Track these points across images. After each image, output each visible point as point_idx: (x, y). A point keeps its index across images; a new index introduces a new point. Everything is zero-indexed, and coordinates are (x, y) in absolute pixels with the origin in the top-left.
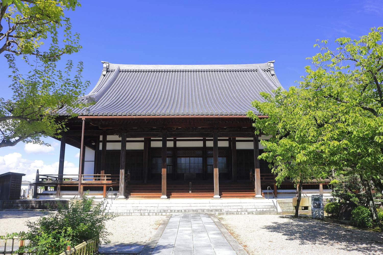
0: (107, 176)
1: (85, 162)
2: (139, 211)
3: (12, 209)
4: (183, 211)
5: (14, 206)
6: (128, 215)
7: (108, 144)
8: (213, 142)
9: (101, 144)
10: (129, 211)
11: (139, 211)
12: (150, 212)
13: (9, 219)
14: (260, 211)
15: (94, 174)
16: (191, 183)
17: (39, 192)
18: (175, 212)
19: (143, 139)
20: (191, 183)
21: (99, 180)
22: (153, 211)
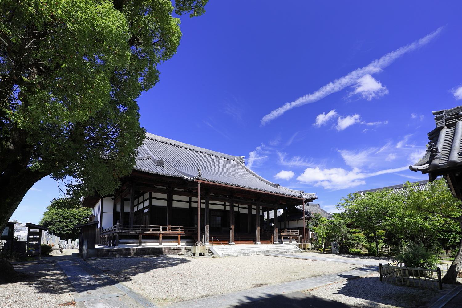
4: (262, 252)
18: (258, 253)
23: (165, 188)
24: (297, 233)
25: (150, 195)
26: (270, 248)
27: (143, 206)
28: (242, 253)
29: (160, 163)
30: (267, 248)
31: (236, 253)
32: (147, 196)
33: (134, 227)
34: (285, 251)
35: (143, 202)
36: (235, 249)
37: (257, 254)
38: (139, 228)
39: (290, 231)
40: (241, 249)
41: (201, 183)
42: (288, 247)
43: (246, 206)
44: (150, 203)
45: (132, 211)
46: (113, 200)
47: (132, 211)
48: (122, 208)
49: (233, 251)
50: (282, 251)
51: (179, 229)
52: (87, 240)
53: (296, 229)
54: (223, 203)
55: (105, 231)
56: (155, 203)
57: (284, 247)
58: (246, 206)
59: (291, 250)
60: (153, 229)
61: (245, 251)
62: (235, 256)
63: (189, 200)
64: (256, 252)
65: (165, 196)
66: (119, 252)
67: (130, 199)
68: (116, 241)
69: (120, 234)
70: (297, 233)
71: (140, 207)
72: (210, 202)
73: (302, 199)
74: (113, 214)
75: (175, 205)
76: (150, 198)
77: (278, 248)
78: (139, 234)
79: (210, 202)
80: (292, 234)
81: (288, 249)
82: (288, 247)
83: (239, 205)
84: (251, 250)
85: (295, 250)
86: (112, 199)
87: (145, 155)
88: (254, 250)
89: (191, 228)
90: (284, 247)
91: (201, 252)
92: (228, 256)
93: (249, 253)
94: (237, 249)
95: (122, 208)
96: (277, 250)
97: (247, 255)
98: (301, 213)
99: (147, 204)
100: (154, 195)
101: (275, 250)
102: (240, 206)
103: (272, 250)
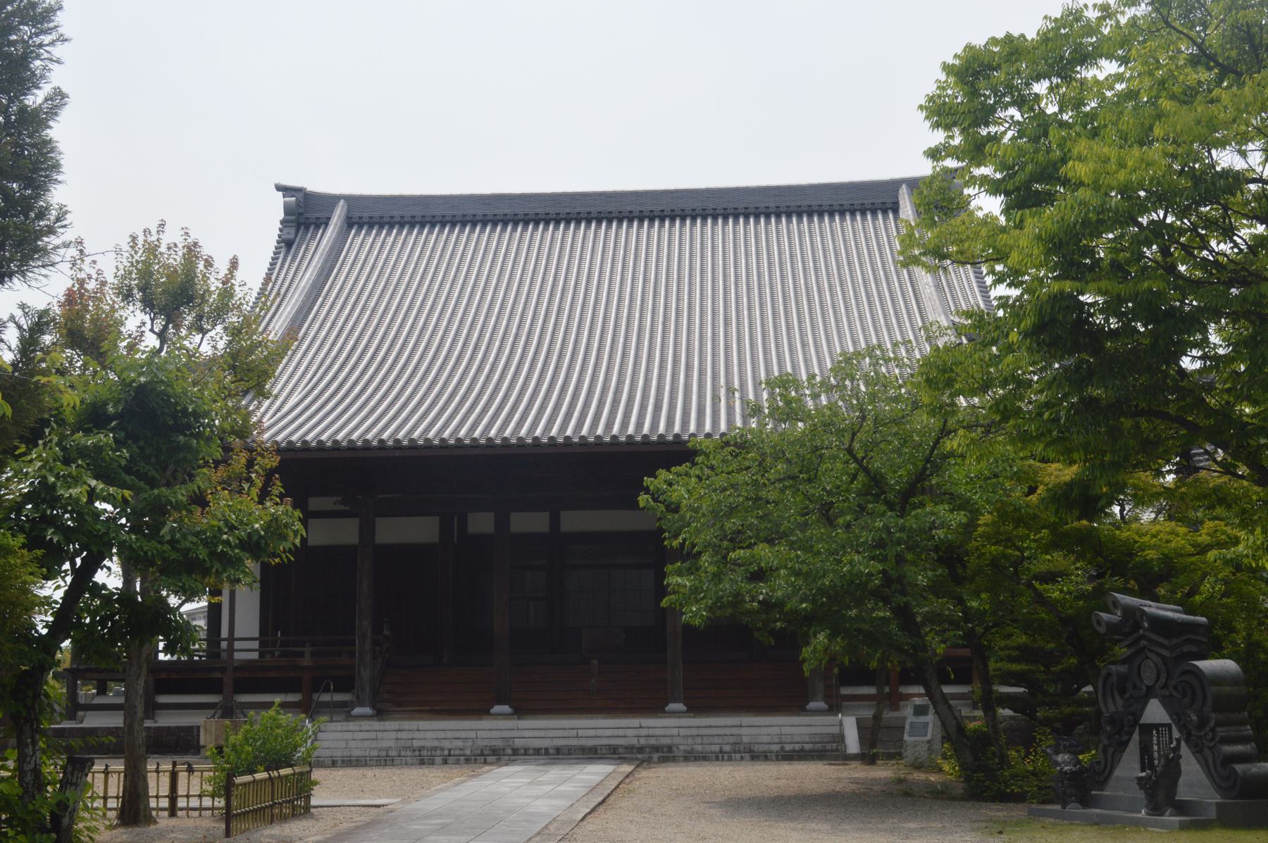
4: (551, 751)
16: (595, 662)
22: (458, 752)
51: (307, 650)
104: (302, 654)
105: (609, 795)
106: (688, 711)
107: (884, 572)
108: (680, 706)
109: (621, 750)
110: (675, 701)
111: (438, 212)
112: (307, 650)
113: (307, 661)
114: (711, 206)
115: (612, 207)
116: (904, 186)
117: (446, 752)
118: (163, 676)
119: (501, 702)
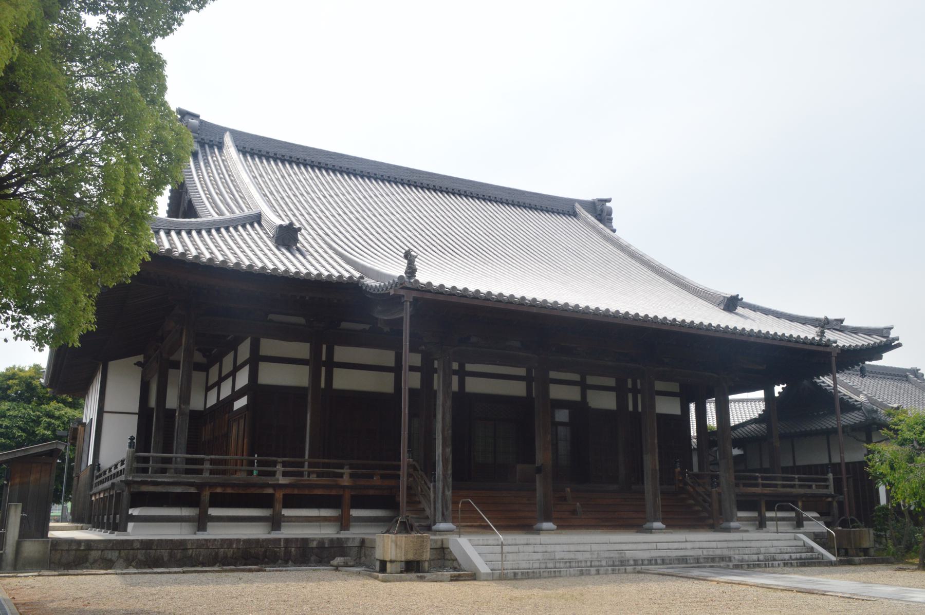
0: (800, 480)
1: (137, 411)
2: (568, 564)
3: (87, 568)
4: (659, 561)
5: (91, 560)
6: (553, 574)
7: (468, 380)
8: (336, 348)
9: (455, 379)
10: (543, 566)
11: (568, 564)
12: (591, 566)
13: (406, 583)
14: (801, 559)
15: (187, 453)
16: (568, 489)
17: (60, 514)
18: (643, 564)
19: (522, 372)
20: (568, 489)
21: (224, 472)
22: (597, 563)
23: (302, 320)
24: (827, 487)
25: (255, 347)
26: (697, 545)
27: (232, 387)
28: (573, 564)
29: (287, 237)
30: (683, 545)
31: (550, 565)
32: (244, 351)
33: (189, 461)
34: (761, 557)
35: (233, 374)
36: (549, 548)
37: (639, 568)
38: (274, 469)
39: (793, 479)
40: (572, 548)
41: (416, 300)
42: (775, 543)
43: (611, 382)
44: (253, 375)
45: (183, 407)
46: (140, 369)
47: (183, 407)
48: (184, 398)
49: (539, 556)
50: (746, 557)
51: (346, 471)
52: (20, 509)
53: (821, 469)
54: (576, 377)
55: (108, 474)
56: (271, 375)
57: (758, 544)
58: (611, 382)
59: (787, 556)
60: (382, 472)
61: (588, 556)
62: (546, 574)
63: (392, 364)
64: (632, 562)
65: (302, 350)
66: (123, 553)
67: (179, 362)
68: (120, 517)
69: (135, 489)
70: (827, 487)
71: (226, 391)
72: (553, 375)
73: (828, 350)
74: (136, 417)
75: (344, 380)
76: (255, 361)
77: (731, 545)
78: (201, 486)
79: (553, 375)
80: (802, 491)
81: (773, 550)
82: (775, 543)
83: (583, 379)
84: (614, 555)
85: (804, 555)
86: (138, 364)
87: (234, 213)
88: (629, 554)
89: (328, 466)
90: (758, 544)
91: (411, 557)
92: (515, 574)
93: (604, 563)
94: (558, 548)
95: (184, 398)
96: (726, 552)
97: (593, 570)
98: (832, 403)
99: (243, 379)
100: (269, 347)
101: (718, 552)
102: (591, 380)
103: (705, 552)
104: (341, 475)
105: (800, 591)
106: (557, 529)
107: (869, 441)
108: (658, 525)
109: (702, 560)
110: (656, 520)
111: (295, 155)
112: (346, 471)
113: (346, 481)
114: (465, 189)
115: (265, 149)
116: (228, 133)
117: (589, 564)
118: (219, 490)
119: (548, 519)
